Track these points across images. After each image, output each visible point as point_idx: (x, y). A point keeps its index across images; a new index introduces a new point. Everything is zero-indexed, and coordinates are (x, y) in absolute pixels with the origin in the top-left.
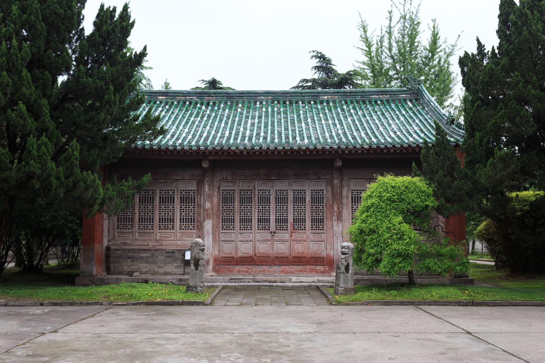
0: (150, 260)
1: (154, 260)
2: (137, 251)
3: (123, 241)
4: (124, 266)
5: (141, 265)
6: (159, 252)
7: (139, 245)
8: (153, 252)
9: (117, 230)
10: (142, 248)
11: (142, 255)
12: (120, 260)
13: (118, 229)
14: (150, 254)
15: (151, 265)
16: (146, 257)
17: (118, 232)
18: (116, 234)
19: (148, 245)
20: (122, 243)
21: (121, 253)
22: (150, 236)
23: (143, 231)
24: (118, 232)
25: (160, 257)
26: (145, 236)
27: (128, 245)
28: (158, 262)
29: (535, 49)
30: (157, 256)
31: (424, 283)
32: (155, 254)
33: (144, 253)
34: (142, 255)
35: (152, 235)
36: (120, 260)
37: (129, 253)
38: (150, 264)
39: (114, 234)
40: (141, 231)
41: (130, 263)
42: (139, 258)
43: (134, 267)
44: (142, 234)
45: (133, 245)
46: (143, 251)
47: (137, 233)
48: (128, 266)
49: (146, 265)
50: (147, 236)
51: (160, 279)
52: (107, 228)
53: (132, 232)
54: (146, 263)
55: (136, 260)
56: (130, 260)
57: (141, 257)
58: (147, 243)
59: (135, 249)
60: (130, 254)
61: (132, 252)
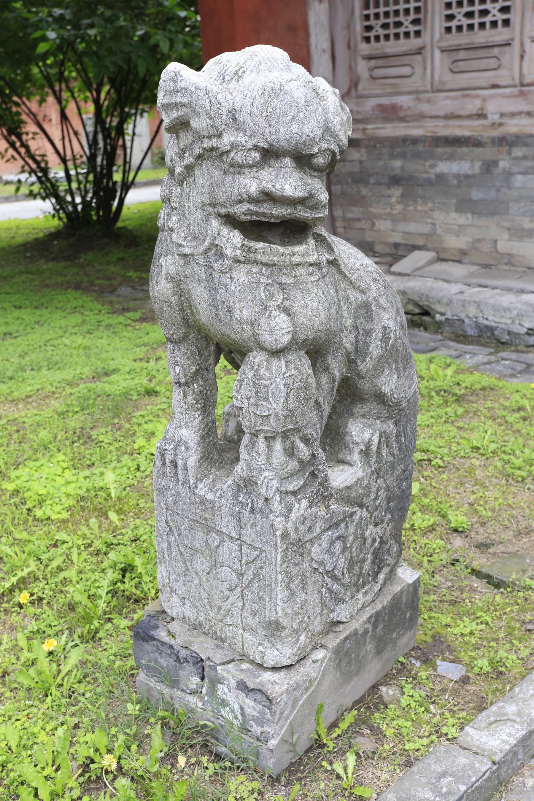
0: (476, 194)
1: (493, 194)
2: (420, 148)
3: (385, 101)
4: (379, 216)
5: (439, 216)
6: (518, 152)
7: (447, 117)
8: (488, 153)
9: (364, 48)
10: (443, 132)
11: (443, 167)
12: (364, 191)
13: (367, 40)
14: (478, 164)
15: (483, 221)
16: (457, 176)
17: (370, 58)
18: (362, 67)
19: (481, 115)
20: (382, 108)
21: (364, 158)
22: (493, 62)
23: (464, 39)
24: (370, 58)
25: (519, 180)
26: (475, 64)
27: (402, 119)
28: (514, 207)
29: (521, 703)
30: (509, 175)
31: (80, 137)
32: (495, 163)
33: (451, 158)
34: (443, 167)
35: (505, 60)
36: (364, 191)
37: (392, 157)
38: (477, 213)
39: (351, 69)
40: (455, 39)
41: (399, 207)
42: (429, 183)
43: (412, 227)
44: (462, 55)
45: (422, 116)
46: (449, 150)
47: (437, 54)
48: (395, 220)
49: (463, 219)
50: (484, 64)
51: (478, 304)
52: (325, 44)
53: (419, 51)
54: (460, 209)
55: (420, 190)
56: (396, 192)
57: (440, 177)
58: (478, 103)
59: (415, 141)
60: (397, 164)
61: (403, 156)
